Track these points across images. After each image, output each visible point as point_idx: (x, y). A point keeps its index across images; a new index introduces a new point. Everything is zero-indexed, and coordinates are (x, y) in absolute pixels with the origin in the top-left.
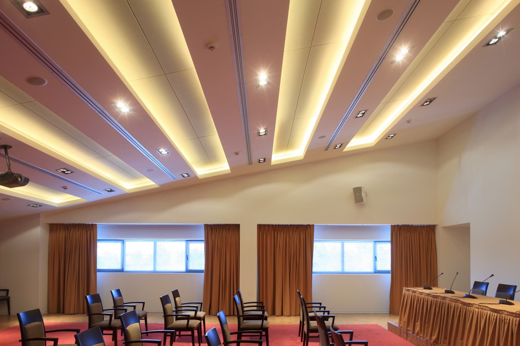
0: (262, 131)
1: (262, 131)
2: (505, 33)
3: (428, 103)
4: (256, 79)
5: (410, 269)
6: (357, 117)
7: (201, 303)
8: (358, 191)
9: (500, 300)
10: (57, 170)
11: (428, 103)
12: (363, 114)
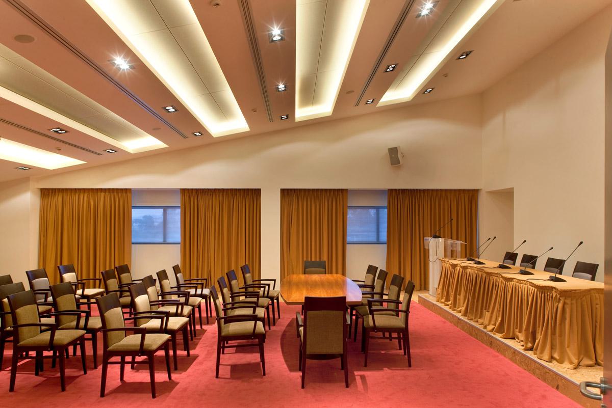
0: (281, 87)
1: (281, 87)
2: (432, 5)
3: (464, 56)
4: (114, 63)
5: (316, 231)
6: (387, 71)
7: (206, 279)
8: (393, 151)
9: (551, 277)
10: (49, 130)
11: (464, 56)
12: (393, 68)
